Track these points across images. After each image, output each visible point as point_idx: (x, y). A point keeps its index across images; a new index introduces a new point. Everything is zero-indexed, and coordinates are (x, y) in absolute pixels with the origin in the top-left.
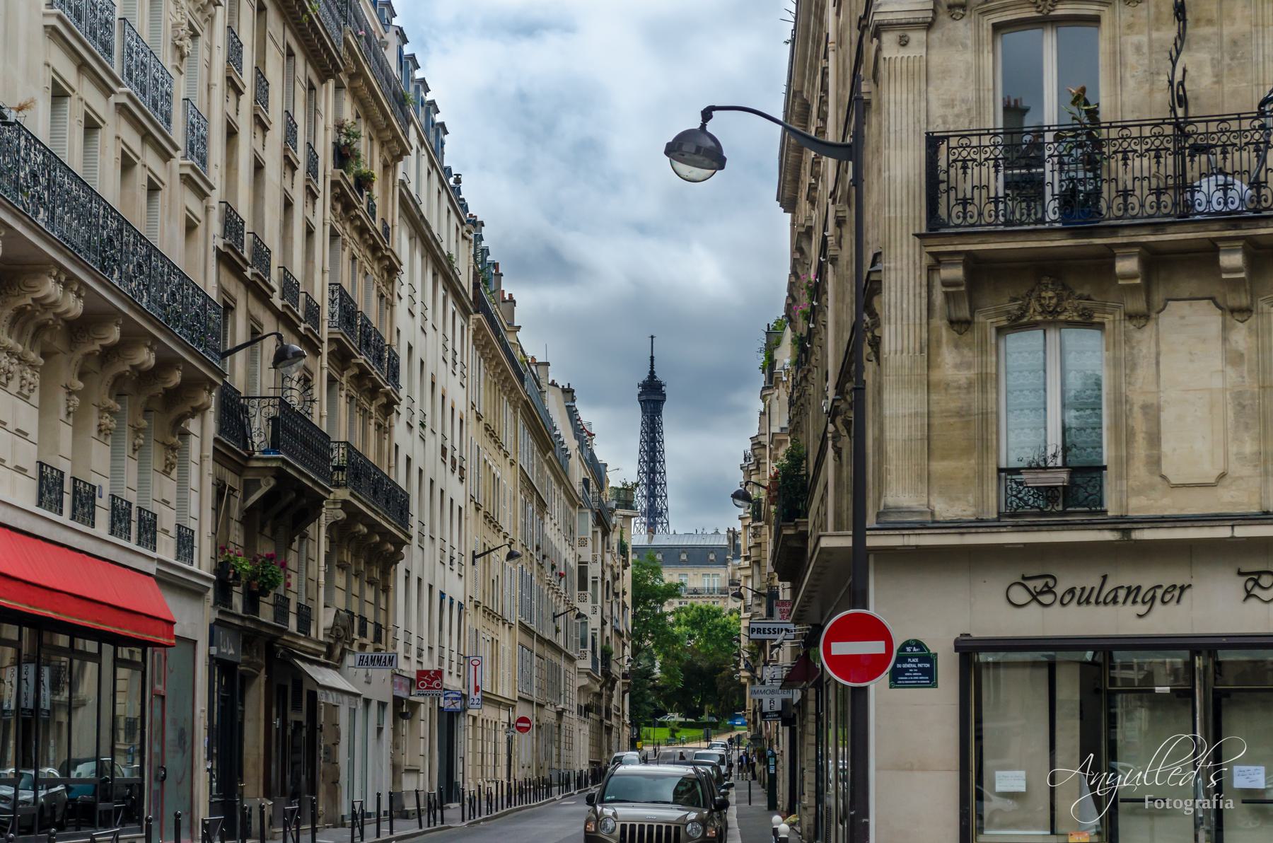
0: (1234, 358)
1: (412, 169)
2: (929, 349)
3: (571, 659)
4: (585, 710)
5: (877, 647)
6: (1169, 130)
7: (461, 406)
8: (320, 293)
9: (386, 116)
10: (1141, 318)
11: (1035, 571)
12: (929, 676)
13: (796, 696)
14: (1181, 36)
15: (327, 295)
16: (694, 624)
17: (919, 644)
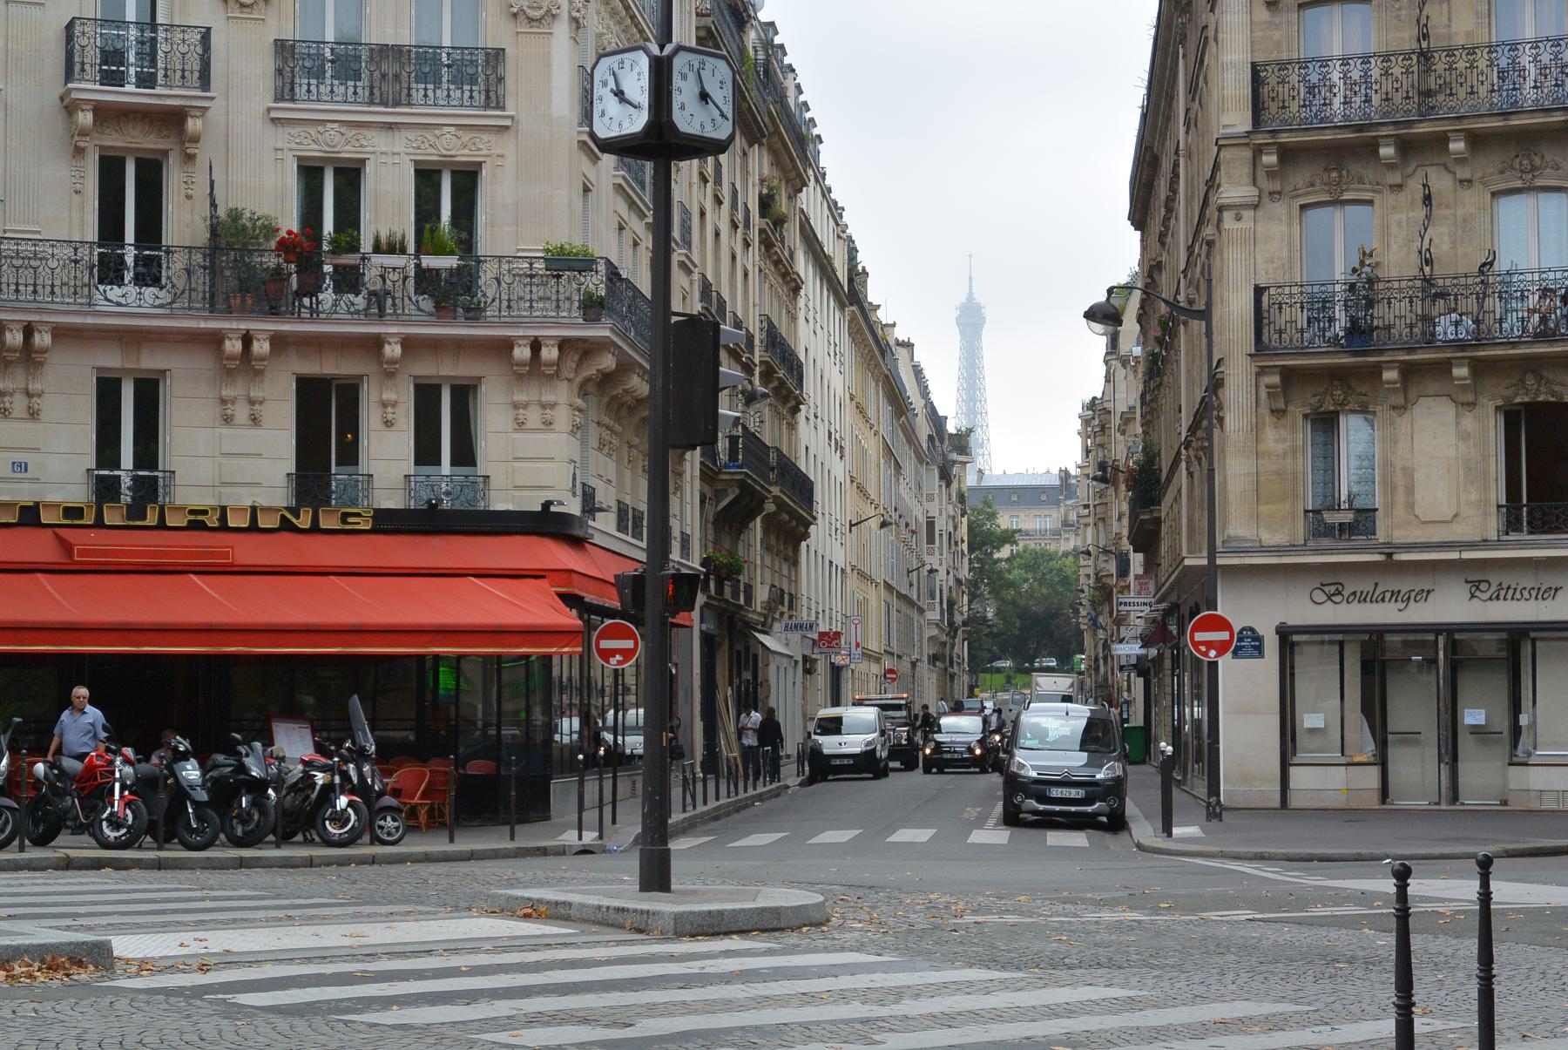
0: (1464, 436)
1: (809, 199)
2: (1257, 429)
3: (921, 611)
4: (934, 659)
5: (1225, 636)
6: (1418, 283)
7: (840, 393)
8: (754, 326)
9: (792, 160)
10: (1402, 409)
11: (1331, 581)
12: (1259, 650)
13: (1153, 652)
14: (1428, 217)
15: (758, 324)
16: (1029, 567)
17: (1252, 629)
